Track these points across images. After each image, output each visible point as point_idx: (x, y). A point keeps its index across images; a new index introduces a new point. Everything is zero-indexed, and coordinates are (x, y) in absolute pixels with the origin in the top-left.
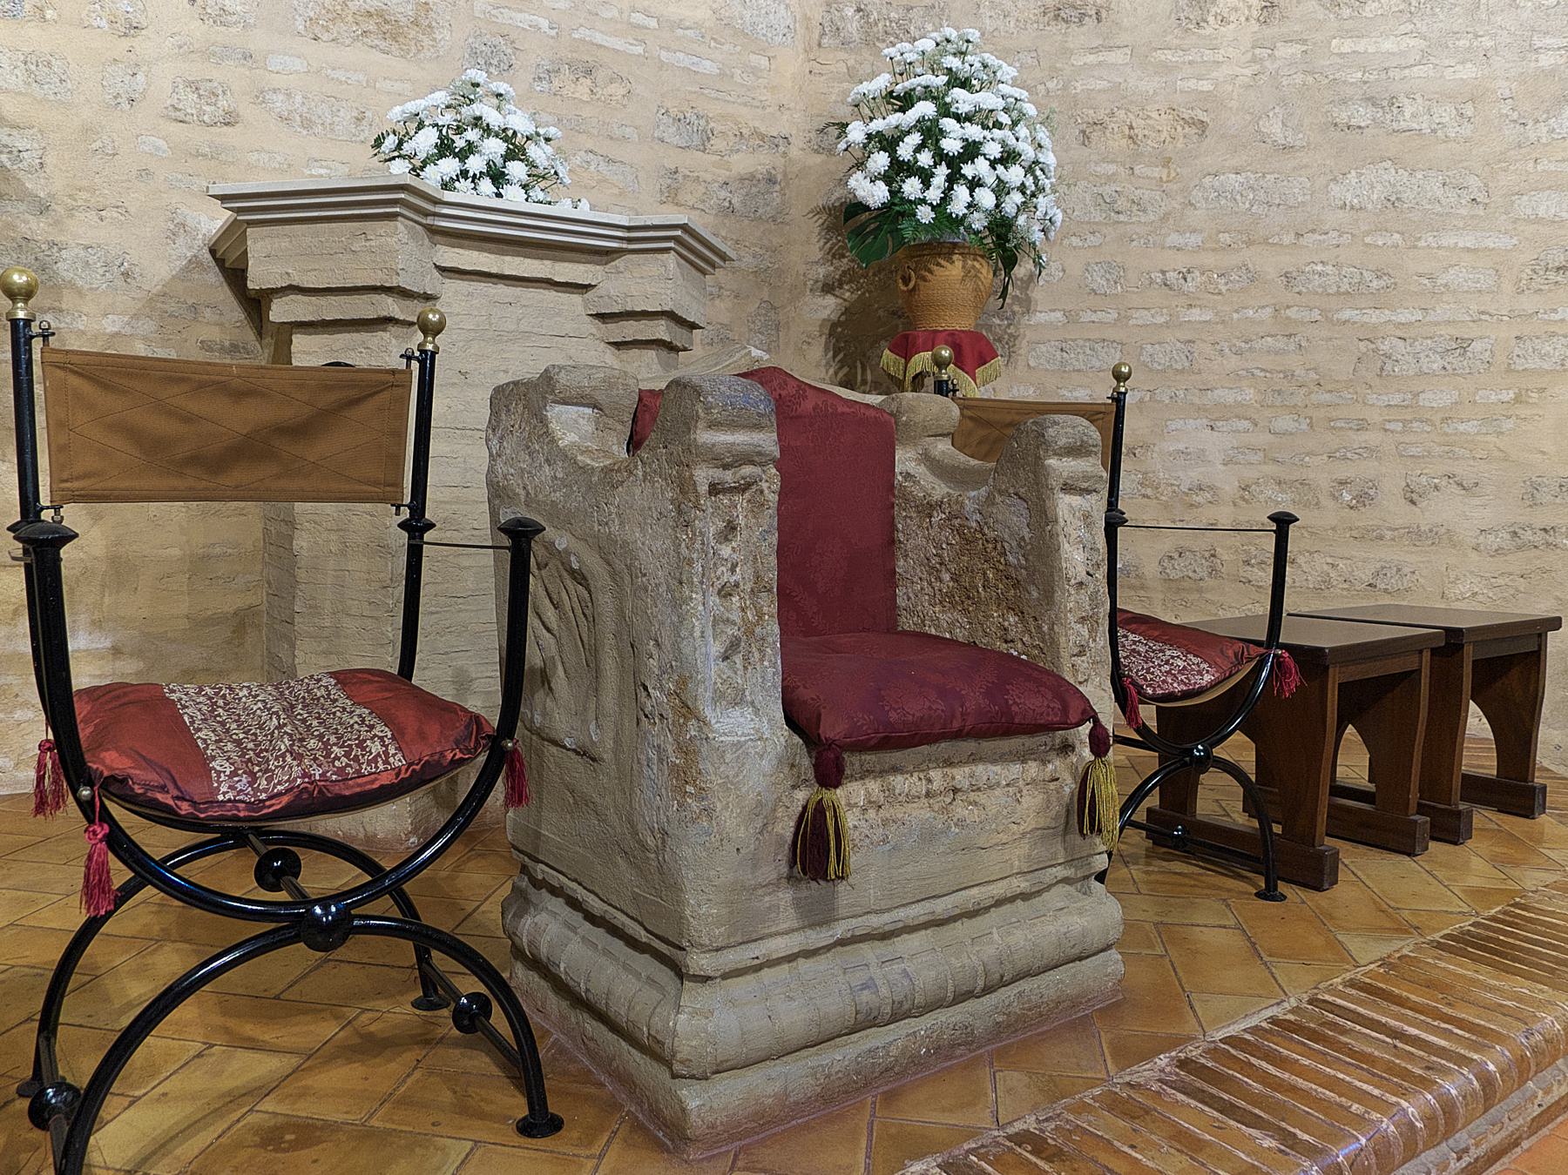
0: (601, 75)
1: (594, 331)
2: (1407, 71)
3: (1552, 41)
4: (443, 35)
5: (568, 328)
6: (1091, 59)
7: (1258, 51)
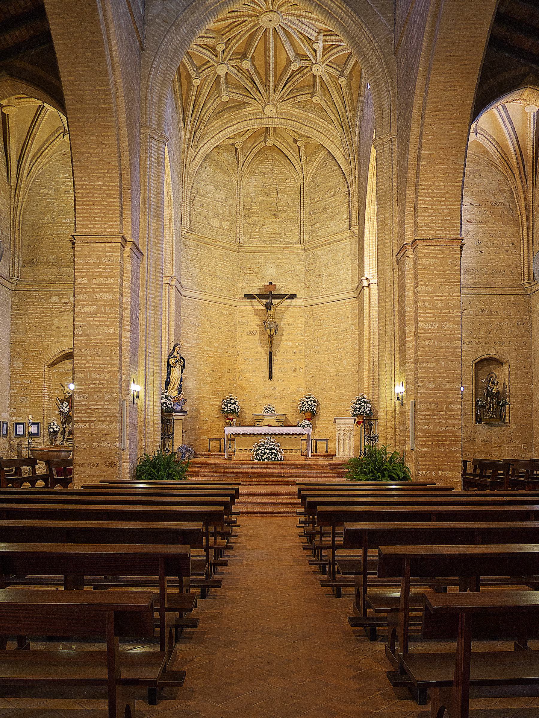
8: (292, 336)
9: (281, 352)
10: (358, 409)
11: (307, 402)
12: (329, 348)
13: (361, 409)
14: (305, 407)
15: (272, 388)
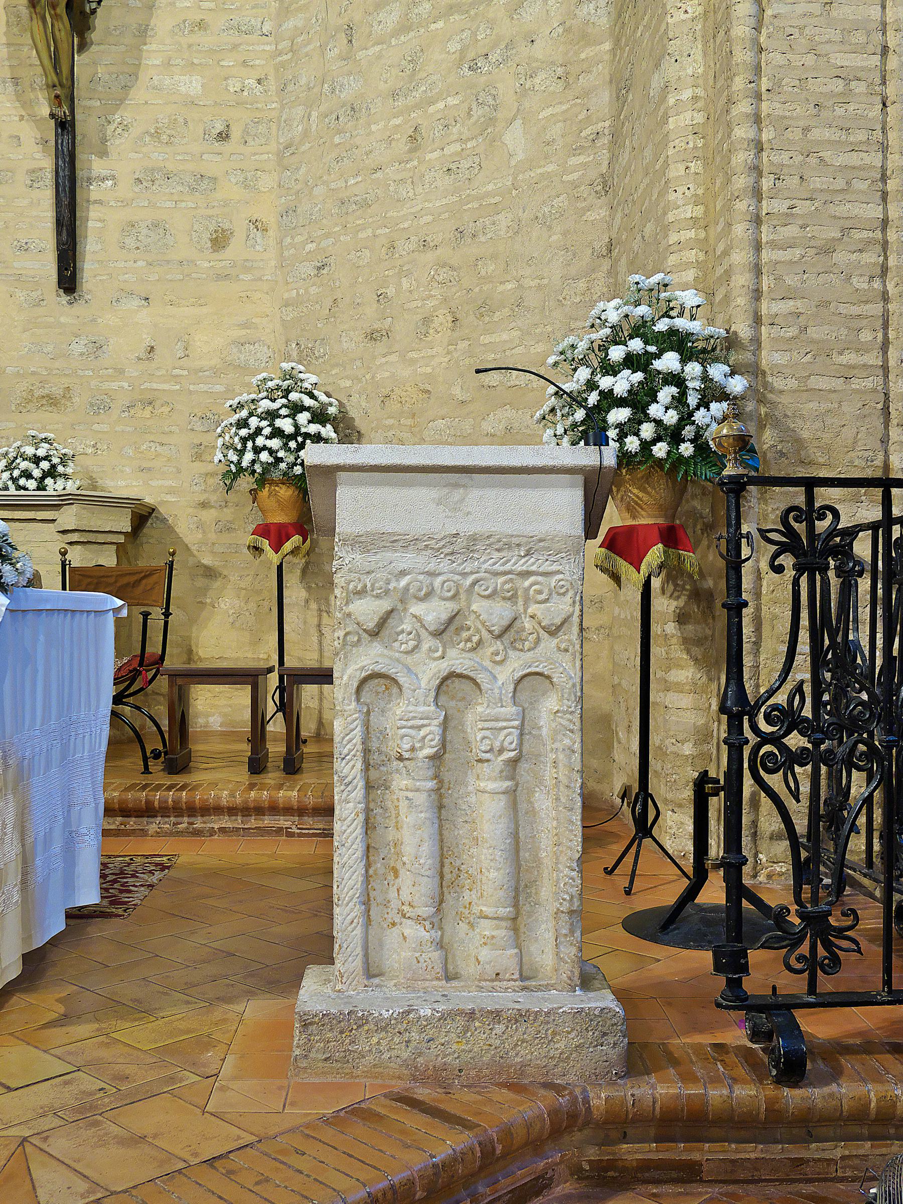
0: (157, 404)
1: (59, 538)
2: (513, 351)
3: (580, 323)
4: (76, 400)
5: (48, 538)
6: (384, 360)
7: (450, 347)
8: (206, 40)
9: (135, 131)
10: (619, 415)
11: (272, 415)
12: (412, 75)
13: (655, 410)
14: (257, 450)
15: (78, 348)
